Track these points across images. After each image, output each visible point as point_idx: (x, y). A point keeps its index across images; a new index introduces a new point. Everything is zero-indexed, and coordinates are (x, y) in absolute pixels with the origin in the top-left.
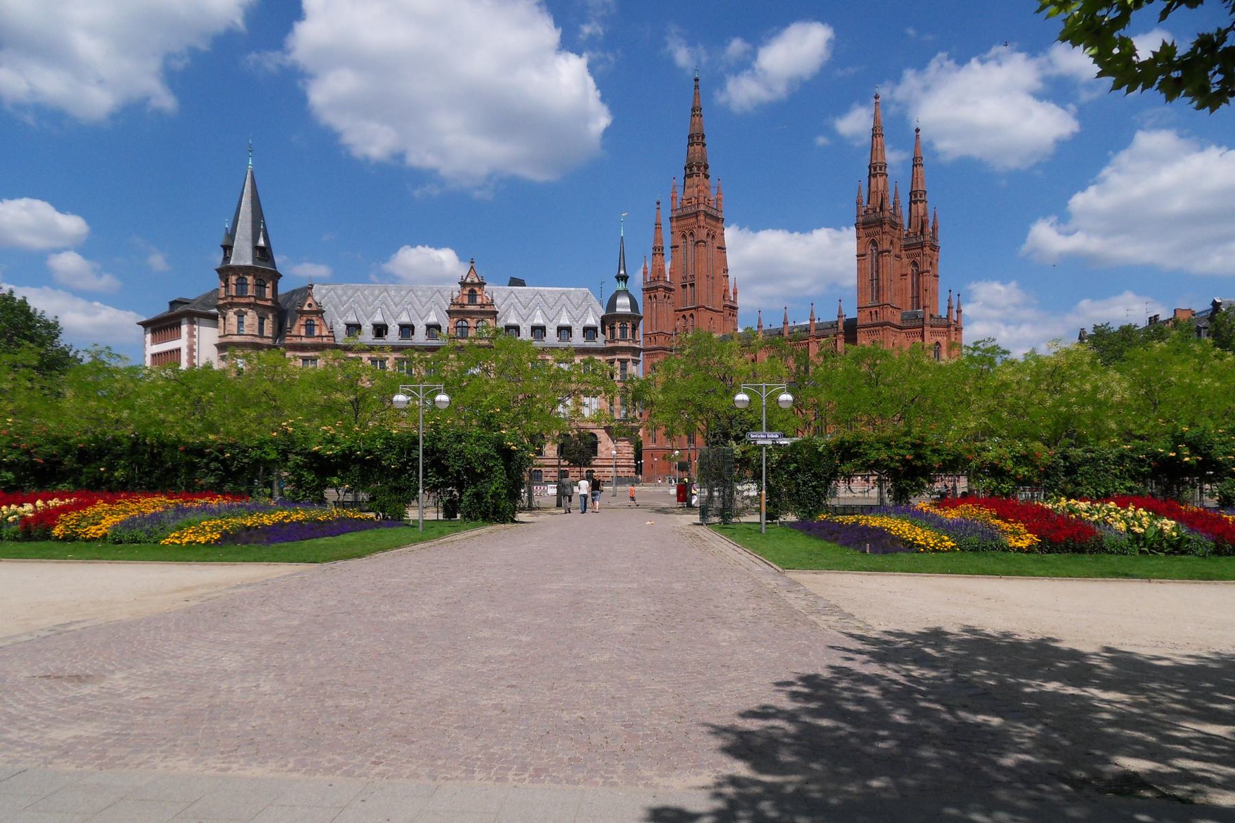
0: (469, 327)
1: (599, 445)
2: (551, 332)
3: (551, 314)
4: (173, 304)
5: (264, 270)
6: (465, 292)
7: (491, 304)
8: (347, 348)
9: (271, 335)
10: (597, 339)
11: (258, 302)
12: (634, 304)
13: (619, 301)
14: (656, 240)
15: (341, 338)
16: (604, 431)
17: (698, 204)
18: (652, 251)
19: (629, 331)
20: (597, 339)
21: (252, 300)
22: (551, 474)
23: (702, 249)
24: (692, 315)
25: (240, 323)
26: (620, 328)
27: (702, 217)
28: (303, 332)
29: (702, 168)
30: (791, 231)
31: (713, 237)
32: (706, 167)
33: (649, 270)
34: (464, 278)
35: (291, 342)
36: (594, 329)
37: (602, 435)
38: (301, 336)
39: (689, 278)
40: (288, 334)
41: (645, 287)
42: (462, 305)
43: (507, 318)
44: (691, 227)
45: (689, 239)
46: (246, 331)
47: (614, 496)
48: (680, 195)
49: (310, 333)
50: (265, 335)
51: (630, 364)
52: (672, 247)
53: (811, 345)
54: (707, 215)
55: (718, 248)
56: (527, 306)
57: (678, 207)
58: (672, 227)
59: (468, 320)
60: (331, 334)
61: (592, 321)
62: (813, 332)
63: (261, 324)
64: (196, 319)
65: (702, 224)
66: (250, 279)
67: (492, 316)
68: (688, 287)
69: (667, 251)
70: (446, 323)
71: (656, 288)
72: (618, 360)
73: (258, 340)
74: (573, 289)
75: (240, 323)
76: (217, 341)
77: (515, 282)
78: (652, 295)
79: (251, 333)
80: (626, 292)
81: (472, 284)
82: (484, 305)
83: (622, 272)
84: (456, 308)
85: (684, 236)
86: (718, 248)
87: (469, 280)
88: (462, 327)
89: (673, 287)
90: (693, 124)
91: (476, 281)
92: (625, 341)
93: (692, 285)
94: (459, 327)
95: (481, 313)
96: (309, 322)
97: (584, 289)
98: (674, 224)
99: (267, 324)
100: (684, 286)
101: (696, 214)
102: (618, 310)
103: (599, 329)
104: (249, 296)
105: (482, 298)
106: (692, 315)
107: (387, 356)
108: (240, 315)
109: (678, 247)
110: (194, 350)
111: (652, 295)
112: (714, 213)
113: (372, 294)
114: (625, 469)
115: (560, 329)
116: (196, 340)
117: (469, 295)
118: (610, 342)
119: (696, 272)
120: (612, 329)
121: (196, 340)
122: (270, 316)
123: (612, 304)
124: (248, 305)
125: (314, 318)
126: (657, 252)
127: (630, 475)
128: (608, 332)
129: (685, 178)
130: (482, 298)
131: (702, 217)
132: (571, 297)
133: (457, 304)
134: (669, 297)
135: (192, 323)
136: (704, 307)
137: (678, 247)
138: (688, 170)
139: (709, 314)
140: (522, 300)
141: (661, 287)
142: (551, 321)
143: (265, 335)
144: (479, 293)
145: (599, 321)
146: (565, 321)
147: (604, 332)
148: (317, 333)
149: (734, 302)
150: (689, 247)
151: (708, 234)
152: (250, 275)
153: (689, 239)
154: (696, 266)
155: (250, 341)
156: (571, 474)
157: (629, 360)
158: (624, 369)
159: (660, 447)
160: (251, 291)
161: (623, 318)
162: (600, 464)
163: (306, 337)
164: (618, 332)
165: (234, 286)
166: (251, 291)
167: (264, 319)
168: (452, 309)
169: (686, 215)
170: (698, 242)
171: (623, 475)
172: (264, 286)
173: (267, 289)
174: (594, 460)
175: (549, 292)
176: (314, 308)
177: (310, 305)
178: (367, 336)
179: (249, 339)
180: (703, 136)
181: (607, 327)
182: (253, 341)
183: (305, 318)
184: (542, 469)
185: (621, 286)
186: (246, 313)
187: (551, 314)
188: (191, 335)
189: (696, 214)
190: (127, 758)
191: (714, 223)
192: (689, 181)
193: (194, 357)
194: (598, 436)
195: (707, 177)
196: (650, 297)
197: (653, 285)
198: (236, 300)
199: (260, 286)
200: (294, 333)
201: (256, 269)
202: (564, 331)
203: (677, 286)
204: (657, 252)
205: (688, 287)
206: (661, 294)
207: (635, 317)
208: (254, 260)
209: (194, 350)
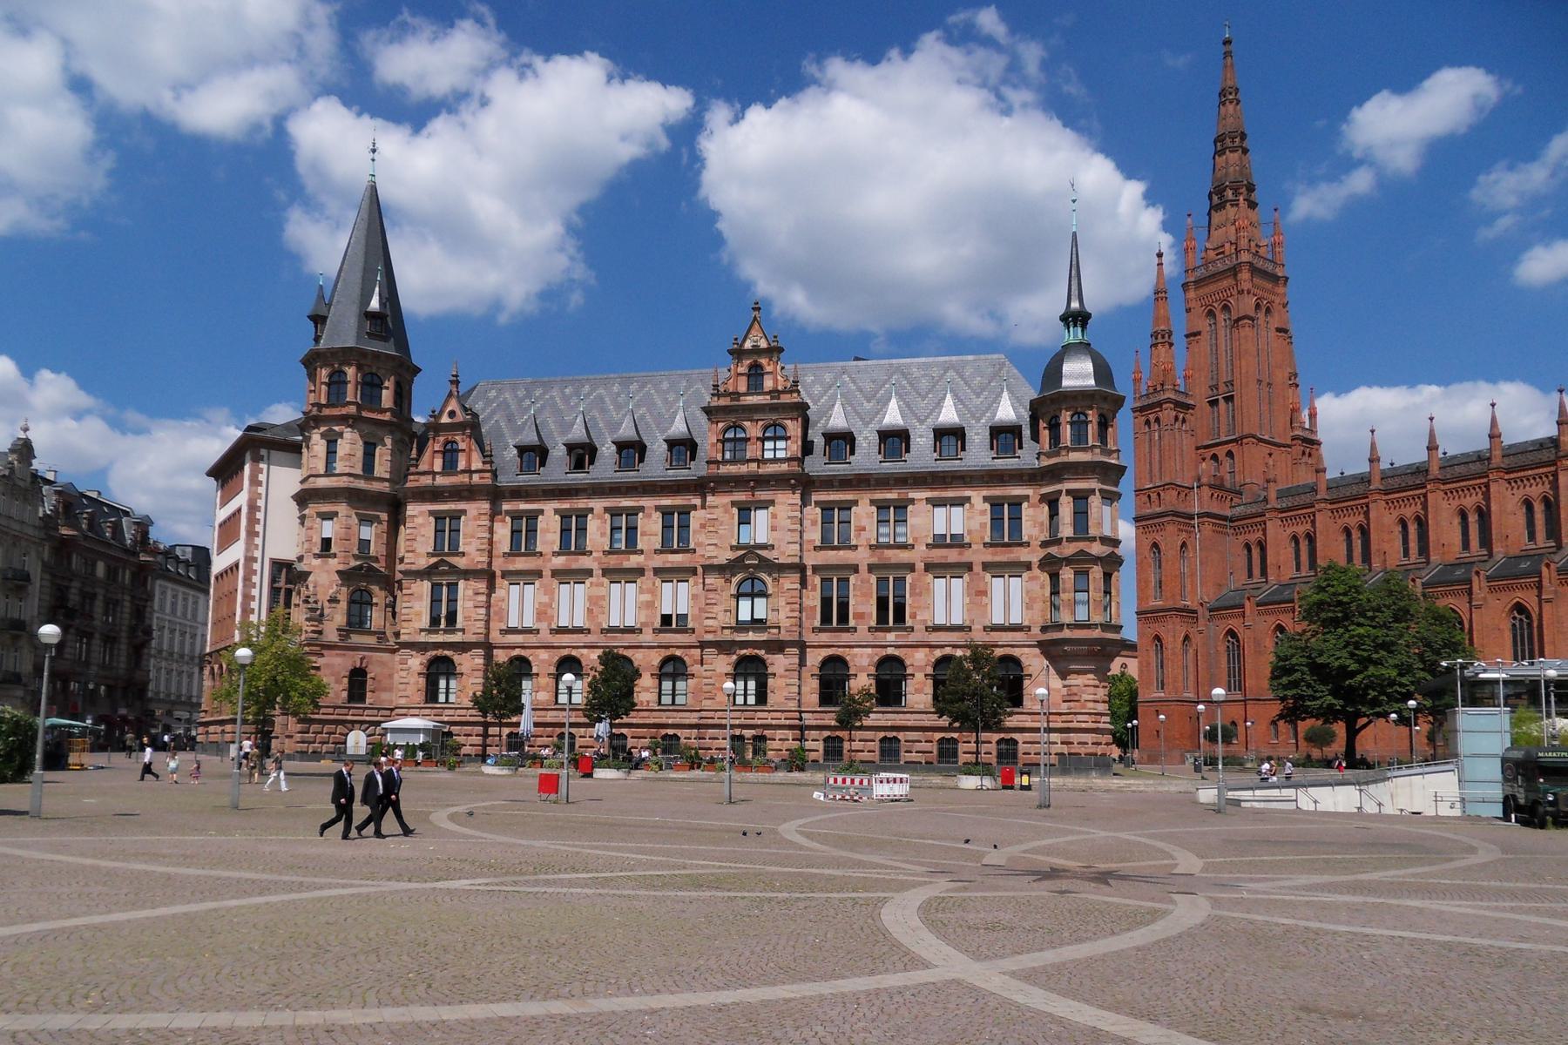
1: (1026, 683)
2: (922, 441)
3: (922, 405)
5: (377, 355)
6: (741, 370)
10: (1019, 452)
11: (364, 414)
12: (1103, 372)
13: (1067, 367)
16: (1037, 651)
17: (1238, 251)
18: (1149, 341)
19: (1092, 430)
20: (1019, 452)
21: (352, 409)
22: (919, 746)
23: (1246, 332)
24: (1230, 454)
25: (331, 453)
26: (1072, 423)
27: (1245, 275)
28: (438, 466)
29: (1243, 190)
30: (1382, 387)
31: (1268, 311)
32: (1251, 188)
33: (1145, 375)
34: (739, 342)
37: (1033, 661)
38: (434, 474)
39: (1222, 388)
40: (412, 469)
41: (1138, 405)
42: (736, 395)
46: (339, 467)
48: (1201, 242)
49: (450, 467)
50: (376, 474)
51: (1095, 501)
52: (1187, 336)
53: (1493, 488)
54: (1254, 270)
55: (1279, 330)
56: (874, 396)
57: (1199, 263)
58: (1187, 301)
59: (747, 424)
61: (1007, 411)
62: (1496, 461)
64: (263, 452)
65: (1246, 286)
66: (351, 372)
67: (795, 414)
68: (1222, 402)
69: (1179, 339)
70: (708, 437)
71: (1159, 404)
72: (1069, 492)
73: (361, 484)
74: (970, 358)
75: (331, 453)
76: (297, 488)
77: (857, 359)
78: (1152, 417)
79: (347, 470)
80: (1084, 348)
81: (756, 351)
83: (1075, 305)
84: (724, 402)
85: (1211, 314)
86: (1279, 330)
87: (748, 345)
88: (735, 440)
89: (1192, 402)
90: (1222, 118)
91: (763, 344)
92: (1084, 450)
93: (1229, 399)
94: (729, 440)
95: (773, 408)
96: (449, 447)
98: (1192, 294)
100: (1213, 403)
101: (1234, 271)
102: (1067, 383)
103: (1026, 432)
105: (776, 381)
106: (1230, 454)
107: (590, 505)
108: (331, 443)
109: (1199, 333)
110: (258, 509)
111: (1152, 417)
112: (1269, 267)
114: (1088, 737)
115: (940, 433)
116: (262, 490)
117: (749, 376)
118: (1049, 455)
119: (1237, 374)
120: (1054, 427)
121: (262, 490)
122: (388, 441)
123: (1053, 372)
124: (343, 419)
125: (458, 438)
126: (1160, 340)
127: (1099, 750)
130: (776, 381)
131: (1245, 275)
133: (727, 394)
134: (1184, 421)
135: (257, 459)
136: (1253, 436)
137: (1199, 333)
138: (1215, 198)
139: (1266, 449)
141: (1169, 401)
144: (769, 369)
145: (1026, 415)
147: (1035, 437)
148: (462, 465)
149: (1312, 430)
150: (1222, 333)
151: (1258, 306)
152: (350, 365)
154: (1237, 363)
155: (345, 485)
156: (962, 747)
157: (1092, 491)
158: (1081, 515)
159: (1173, 696)
160: (351, 393)
161: (1079, 398)
162: (1028, 725)
164: (1067, 432)
166: (351, 393)
167: (375, 446)
168: (713, 404)
169: (1213, 275)
170: (1237, 321)
171: (1082, 750)
172: (380, 387)
173: (384, 392)
174: (1010, 714)
175: (919, 366)
177: (452, 414)
178: (557, 470)
180: (1243, 136)
181: (1042, 424)
182: (352, 485)
184: (901, 736)
185: (1074, 335)
186: (341, 435)
188: (255, 482)
189: (1234, 271)
190: (1359, 678)
191: (1269, 286)
192: (1217, 217)
194: (1025, 661)
195: (1252, 205)
196: (1148, 422)
197: (1153, 399)
198: (326, 412)
199: (371, 386)
201: (363, 354)
202: (949, 437)
203: (1199, 396)
204: (1160, 340)
205: (1222, 402)
206: (1168, 414)
207: (1105, 397)
208: (359, 338)
209: (258, 509)
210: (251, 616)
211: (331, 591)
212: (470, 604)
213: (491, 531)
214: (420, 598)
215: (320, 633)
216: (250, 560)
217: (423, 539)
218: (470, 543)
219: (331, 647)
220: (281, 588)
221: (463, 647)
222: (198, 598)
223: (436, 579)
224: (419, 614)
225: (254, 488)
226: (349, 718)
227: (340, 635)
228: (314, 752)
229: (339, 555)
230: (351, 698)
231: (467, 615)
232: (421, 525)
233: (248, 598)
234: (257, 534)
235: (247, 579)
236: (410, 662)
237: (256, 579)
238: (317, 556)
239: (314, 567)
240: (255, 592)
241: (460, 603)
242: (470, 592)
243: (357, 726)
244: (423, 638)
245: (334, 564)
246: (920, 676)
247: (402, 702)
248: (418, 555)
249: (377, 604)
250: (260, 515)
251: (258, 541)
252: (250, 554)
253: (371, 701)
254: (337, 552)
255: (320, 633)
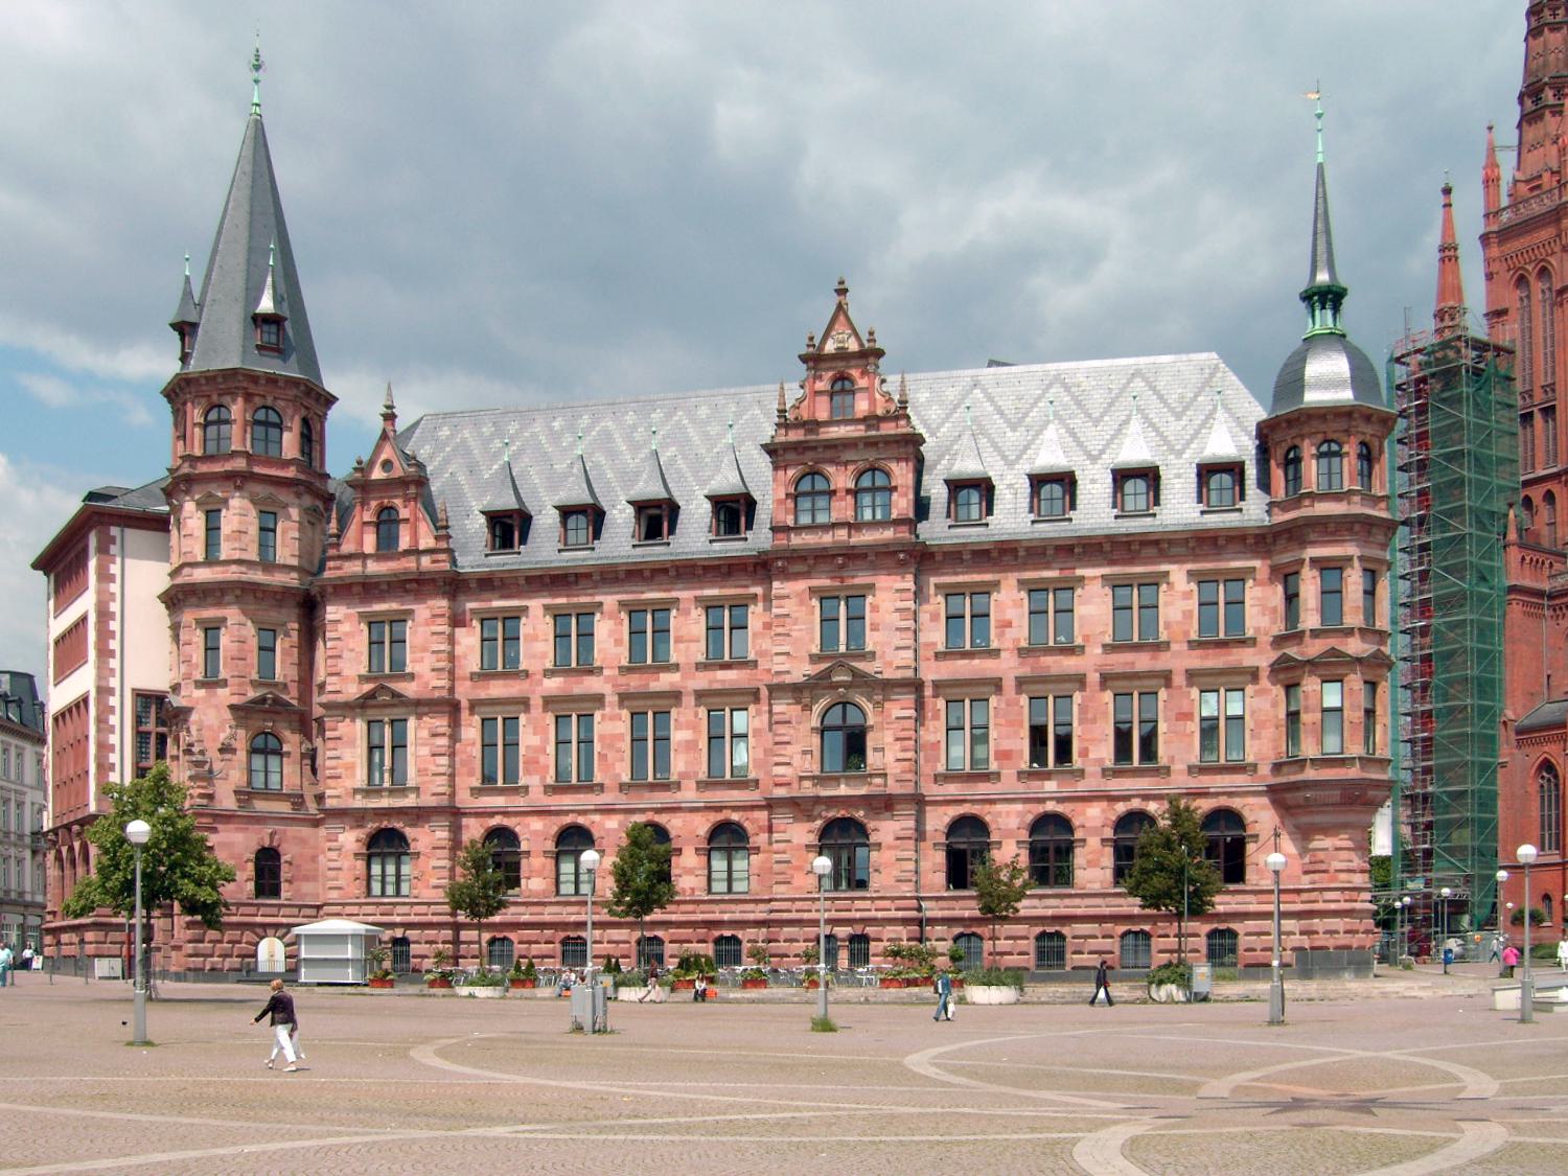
0: (832, 493)
1: (1250, 848)
4: (91, 496)
7: (900, 414)
8: (488, 583)
9: (294, 562)
14: (1442, 296)
15: (475, 554)
16: (1265, 800)
21: (240, 464)
22: (1093, 944)
25: (212, 529)
28: (370, 543)
34: (817, 342)
35: (338, 573)
36: (1235, 469)
37: (1260, 816)
38: (364, 557)
42: (813, 425)
43: (953, 459)
44: (1540, 254)
45: (1537, 286)
47: (1276, 1022)
49: (387, 546)
56: (1021, 420)
58: (1488, 261)
60: (443, 545)
61: (1231, 441)
63: (266, 530)
68: (1538, 417)
72: (1314, 561)
73: (258, 576)
75: (212, 529)
76: (164, 583)
79: (237, 555)
80: (1338, 339)
81: (842, 355)
82: (881, 419)
83: (1323, 277)
84: (795, 436)
87: (830, 347)
91: (853, 346)
93: (1549, 411)
95: (870, 443)
96: (384, 516)
97: (1204, 356)
98: (1495, 251)
99: (284, 532)
103: (1251, 472)
104: (234, 454)
105: (873, 401)
106: (1549, 497)
110: (112, 616)
113: (571, 427)
116: (115, 588)
121: (115, 588)
122: (294, 513)
123: (1291, 381)
127: (1355, 941)
128: (1278, 475)
129: (1519, 126)
130: (873, 401)
132: (1160, 385)
138: (1528, 102)
140: (1007, 405)
142: (1094, 459)
143: (280, 560)
144: (862, 383)
146: (1135, 452)
147: (1265, 484)
148: (404, 543)
153: (1537, 286)
155: (235, 577)
157: (1349, 559)
163: (379, 556)
165: (197, 430)
171: (1330, 942)
176: (398, 471)
179: (232, 574)
182: (244, 578)
183: (374, 504)
184: (512, 936)
185: (1324, 320)
187: (1094, 438)
188: (105, 577)
192: (1532, 133)
193: (112, 634)
194: (1249, 816)
200: (347, 547)
205: (1538, 417)
207: (1368, 416)
209: (112, 616)
210: (111, 774)
211: (222, 736)
212: (425, 751)
213: (452, 640)
214: (352, 743)
215: (211, 797)
216: (104, 691)
217: (354, 654)
218: (421, 660)
219: (227, 817)
220: (150, 733)
221: (419, 815)
222: (23, 749)
223: (373, 714)
224: (351, 767)
225: (104, 585)
226: (259, 919)
227: (239, 800)
228: (212, 969)
229: (231, 681)
230: (260, 891)
231: (422, 766)
232: (347, 634)
233: (104, 748)
234: (112, 654)
235: (101, 720)
236: (341, 837)
237: (114, 720)
238: (199, 684)
239: (198, 699)
240: (114, 739)
241: (410, 749)
242: (425, 733)
243: (270, 931)
244: (359, 802)
245: (225, 695)
246: (1094, 842)
247: (334, 895)
248: (346, 680)
249: (289, 753)
250: (114, 626)
251: (114, 663)
252: (103, 684)
253: (289, 895)
254: (227, 677)
255: (211, 797)
